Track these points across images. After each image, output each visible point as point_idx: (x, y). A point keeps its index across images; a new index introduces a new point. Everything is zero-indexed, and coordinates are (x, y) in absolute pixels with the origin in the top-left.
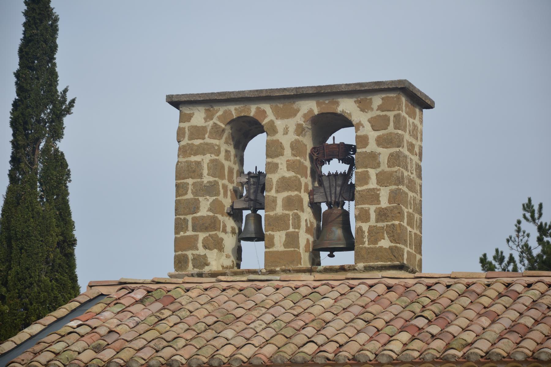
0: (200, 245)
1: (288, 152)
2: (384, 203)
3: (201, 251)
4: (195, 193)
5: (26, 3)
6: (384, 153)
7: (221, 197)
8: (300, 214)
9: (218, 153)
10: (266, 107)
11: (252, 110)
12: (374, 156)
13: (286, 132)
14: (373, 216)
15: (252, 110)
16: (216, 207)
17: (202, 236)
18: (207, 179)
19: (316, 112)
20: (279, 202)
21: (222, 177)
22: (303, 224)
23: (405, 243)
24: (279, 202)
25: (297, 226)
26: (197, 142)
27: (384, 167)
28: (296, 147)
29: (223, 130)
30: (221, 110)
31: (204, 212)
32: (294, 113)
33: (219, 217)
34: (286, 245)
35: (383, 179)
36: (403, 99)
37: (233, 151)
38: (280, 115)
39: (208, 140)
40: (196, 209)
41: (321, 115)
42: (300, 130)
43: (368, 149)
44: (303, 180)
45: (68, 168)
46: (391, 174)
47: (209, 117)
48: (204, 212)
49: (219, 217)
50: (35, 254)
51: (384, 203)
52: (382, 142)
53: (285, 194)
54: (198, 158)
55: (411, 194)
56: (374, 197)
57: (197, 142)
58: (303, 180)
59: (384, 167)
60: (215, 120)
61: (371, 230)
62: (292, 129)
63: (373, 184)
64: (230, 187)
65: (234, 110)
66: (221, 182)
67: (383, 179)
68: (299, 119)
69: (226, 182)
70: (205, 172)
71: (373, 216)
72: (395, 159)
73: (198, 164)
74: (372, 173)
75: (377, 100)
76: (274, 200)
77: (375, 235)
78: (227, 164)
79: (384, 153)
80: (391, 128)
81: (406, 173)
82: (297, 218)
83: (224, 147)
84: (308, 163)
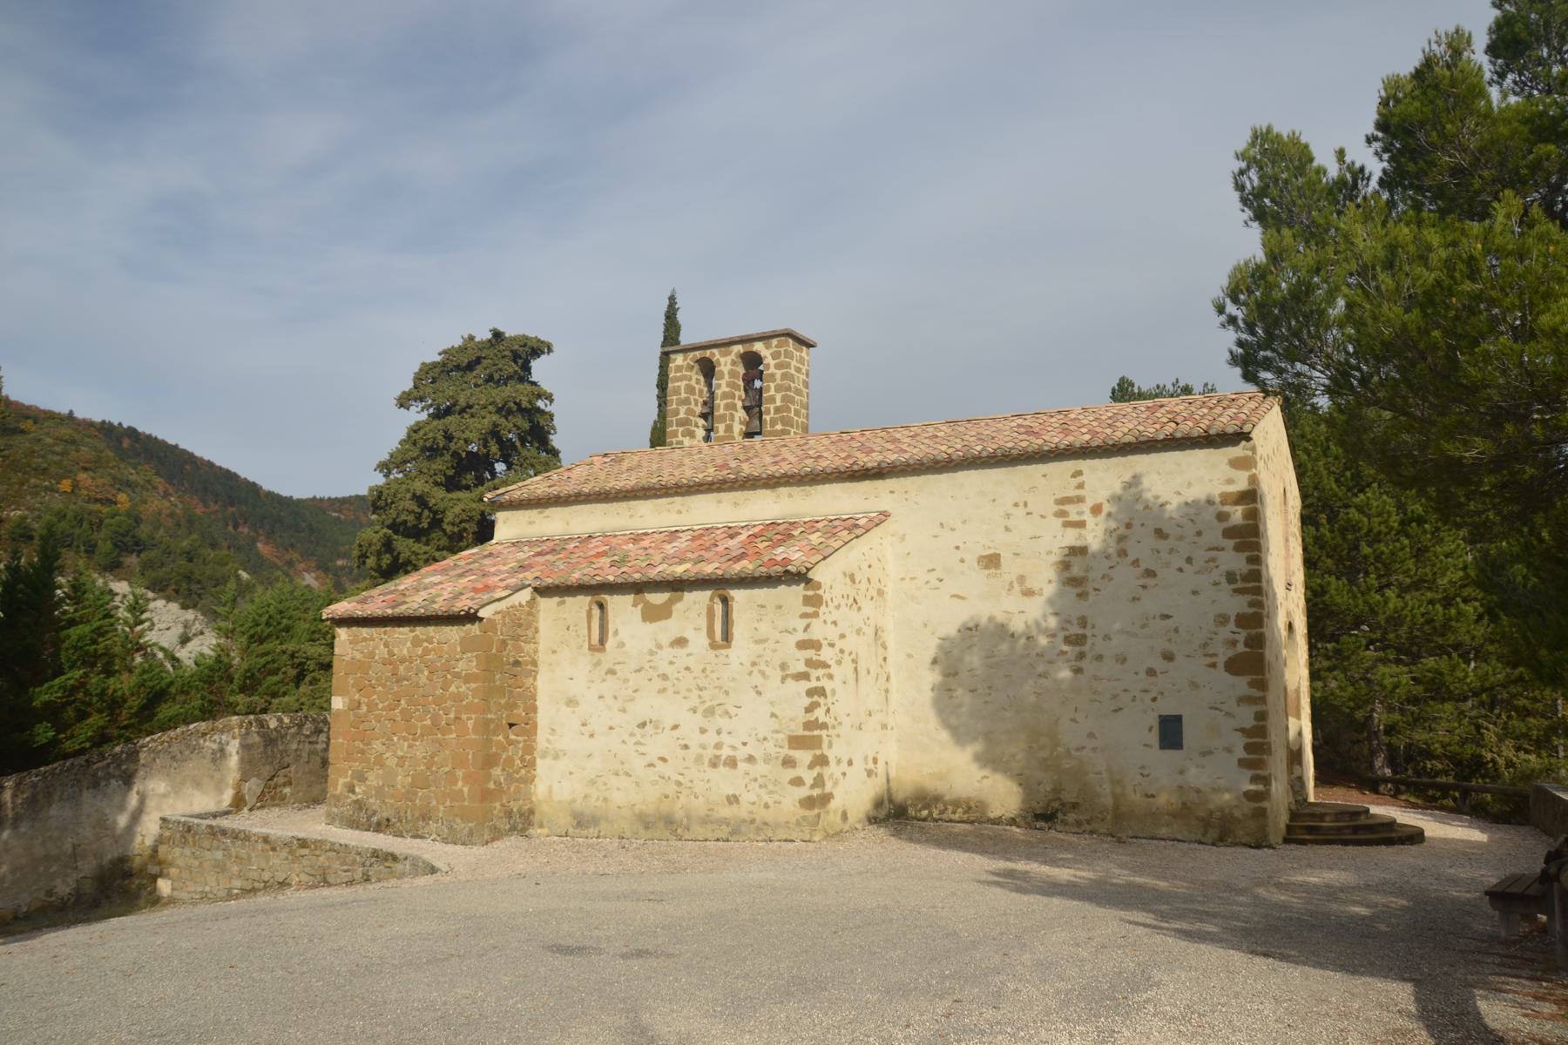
0: (680, 435)
1: (727, 376)
2: (778, 403)
3: (680, 438)
4: (677, 404)
5: (1494, 5)
6: (779, 373)
7: (692, 406)
8: (734, 413)
9: (690, 379)
10: (715, 351)
11: (708, 353)
12: (773, 375)
13: (725, 365)
14: (772, 411)
15: (708, 353)
16: (690, 412)
17: (681, 429)
18: (684, 395)
19: (742, 351)
20: (722, 407)
21: (694, 394)
22: (737, 419)
23: (792, 427)
24: (722, 407)
25: (732, 419)
26: (679, 374)
27: (778, 381)
28: (732, 374)
29: (693, 367)
30: (691, 355)
31: (682, 415)
32: (729, 353)
33: (691, 418)
34: (725, 432)
35: (778, 389)
36: (791, 341)
37: (702, 379)
38: (723, 355)
39: (684, 373)
40: (678, 414)
41: (745, 353)
42: (734, 363)
43: (770, 372)
44: (737, 393)
45: (379, 480)
46: (782, 385)
47: (685, 359)
48: (682, 415)
49: (691, 418)
50: (1442, 134)
51: (778, 403)
52: (778, 366)
53: (725, 401)
54: (679, 384)
55: (797, 398)
56: (772, 399)
57: (679, 374)
58: (737, 393)
59: (778, 381)
60: (688, 361)
61: (771, 419)
62: (729, 362)
63: (772, 392)
64: (701, 400)
65: (698, 354)
66: (692, 398)
67: (778, 389)
68: (733, 356)
69: (697, 397)
70: (683, 391)
71: (772, 411)
72: (784, 377)
73: (679, 387)
74: (772, 385)
75: (775, 342)
76: (719, 406)
77: (774, 423)
78: (697, 387)
79: (779, 373)
80: (782, 358)
81: (792, 385)
82: (732, 416)
83: (694, 377)
84: (741, 383)
